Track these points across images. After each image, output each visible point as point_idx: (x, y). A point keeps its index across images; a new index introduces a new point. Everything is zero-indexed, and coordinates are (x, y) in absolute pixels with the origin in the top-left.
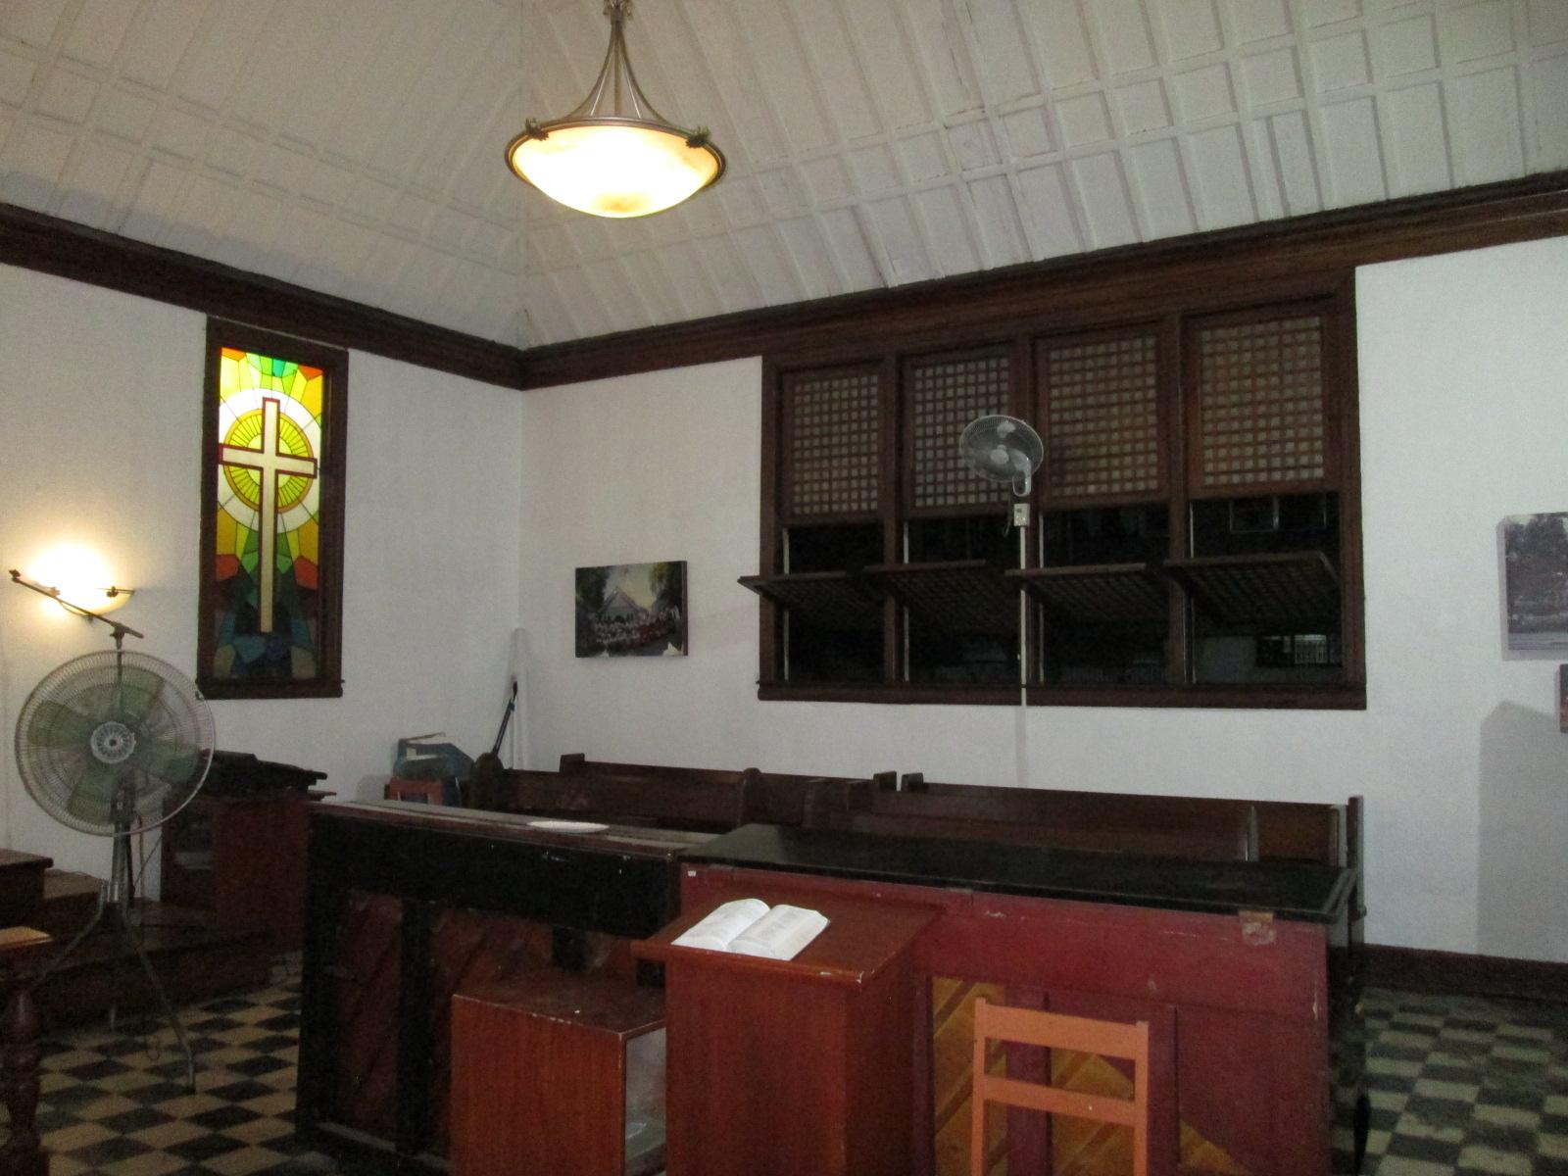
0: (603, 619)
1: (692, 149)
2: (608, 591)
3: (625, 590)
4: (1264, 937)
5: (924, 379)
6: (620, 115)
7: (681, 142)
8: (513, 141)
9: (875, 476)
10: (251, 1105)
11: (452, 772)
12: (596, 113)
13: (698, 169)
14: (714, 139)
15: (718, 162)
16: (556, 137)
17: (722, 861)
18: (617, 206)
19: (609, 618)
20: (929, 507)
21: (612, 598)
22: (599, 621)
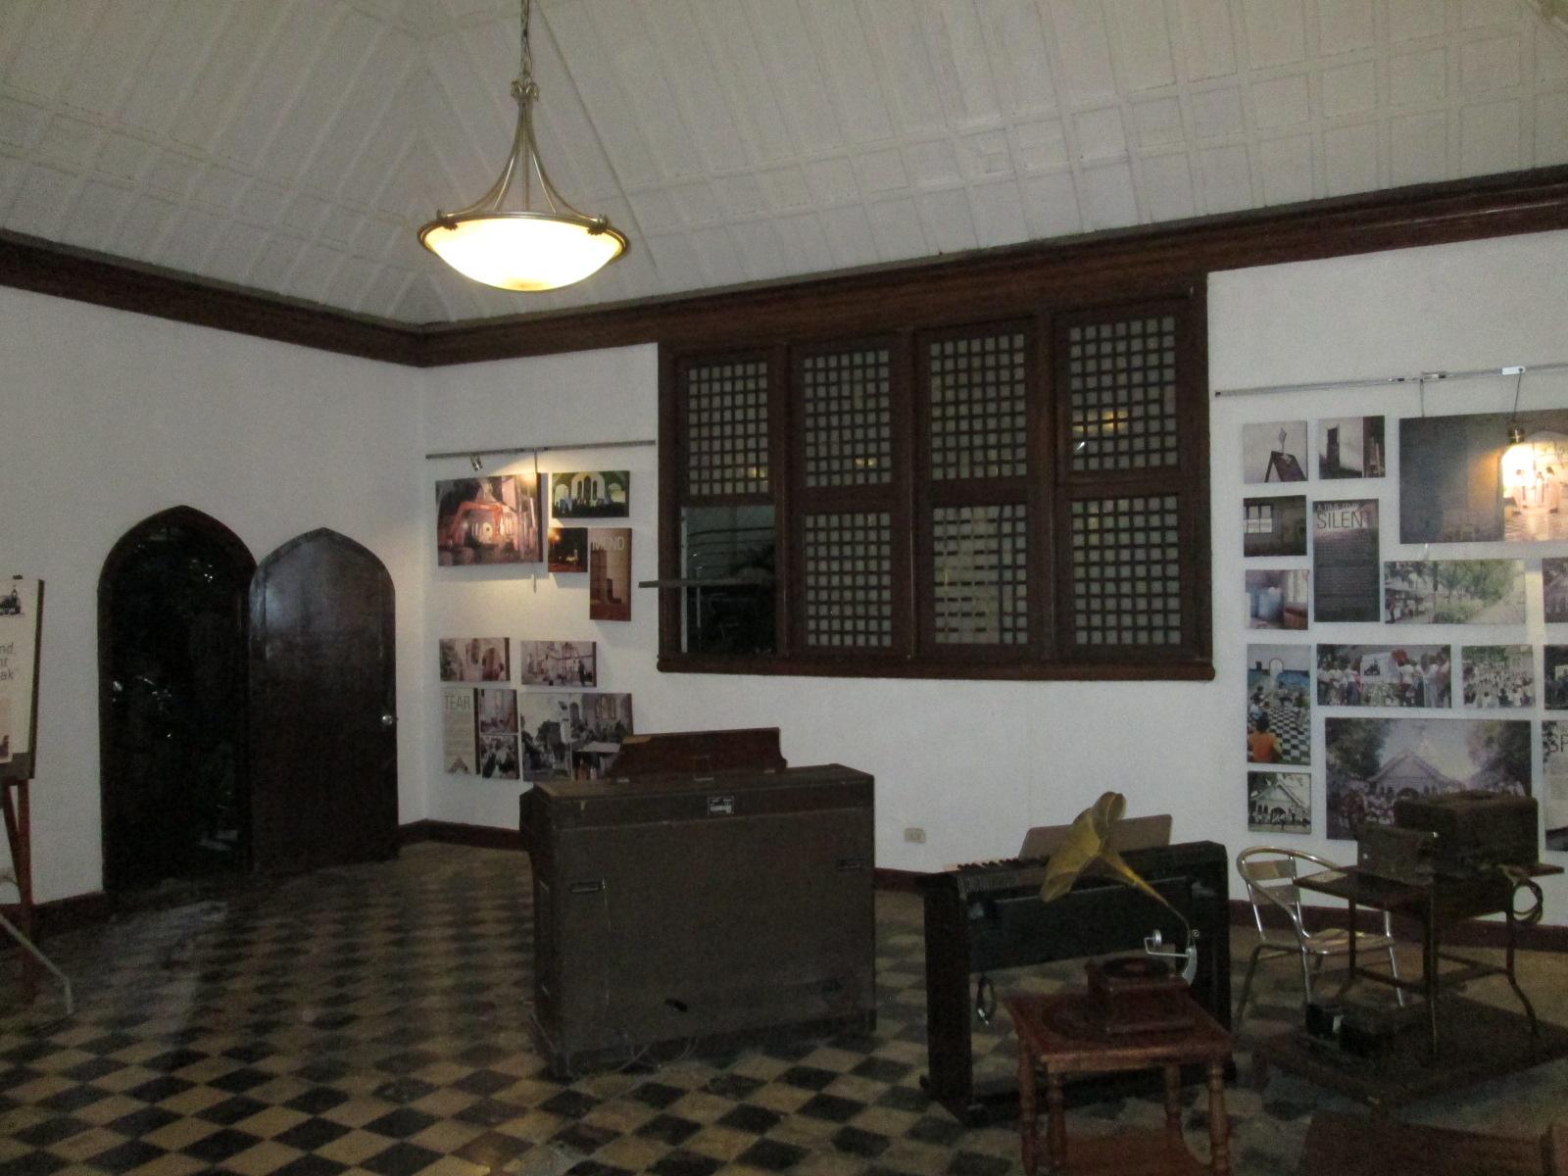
0: (1378, 790)
1: (594, 236)
2: (1385, 756)
3: (1421, 753)
4: (594, 499)
5: (815, 370)
6: (529, 207)
7: (584, 230)
8: (621, 234)
9: (809, 430)
10: (246, 1126)
11: (1228, 1094)
12: (498, 208)
13: (607, 247)
14: (614, 224)
15: (621, 242)
16: (463, 226)
17: (1258, 851)
18: (523, 286)
19: (1390, 790)
20: (1123, 471)
21: (1395, 764)
22: (1371, 792)
